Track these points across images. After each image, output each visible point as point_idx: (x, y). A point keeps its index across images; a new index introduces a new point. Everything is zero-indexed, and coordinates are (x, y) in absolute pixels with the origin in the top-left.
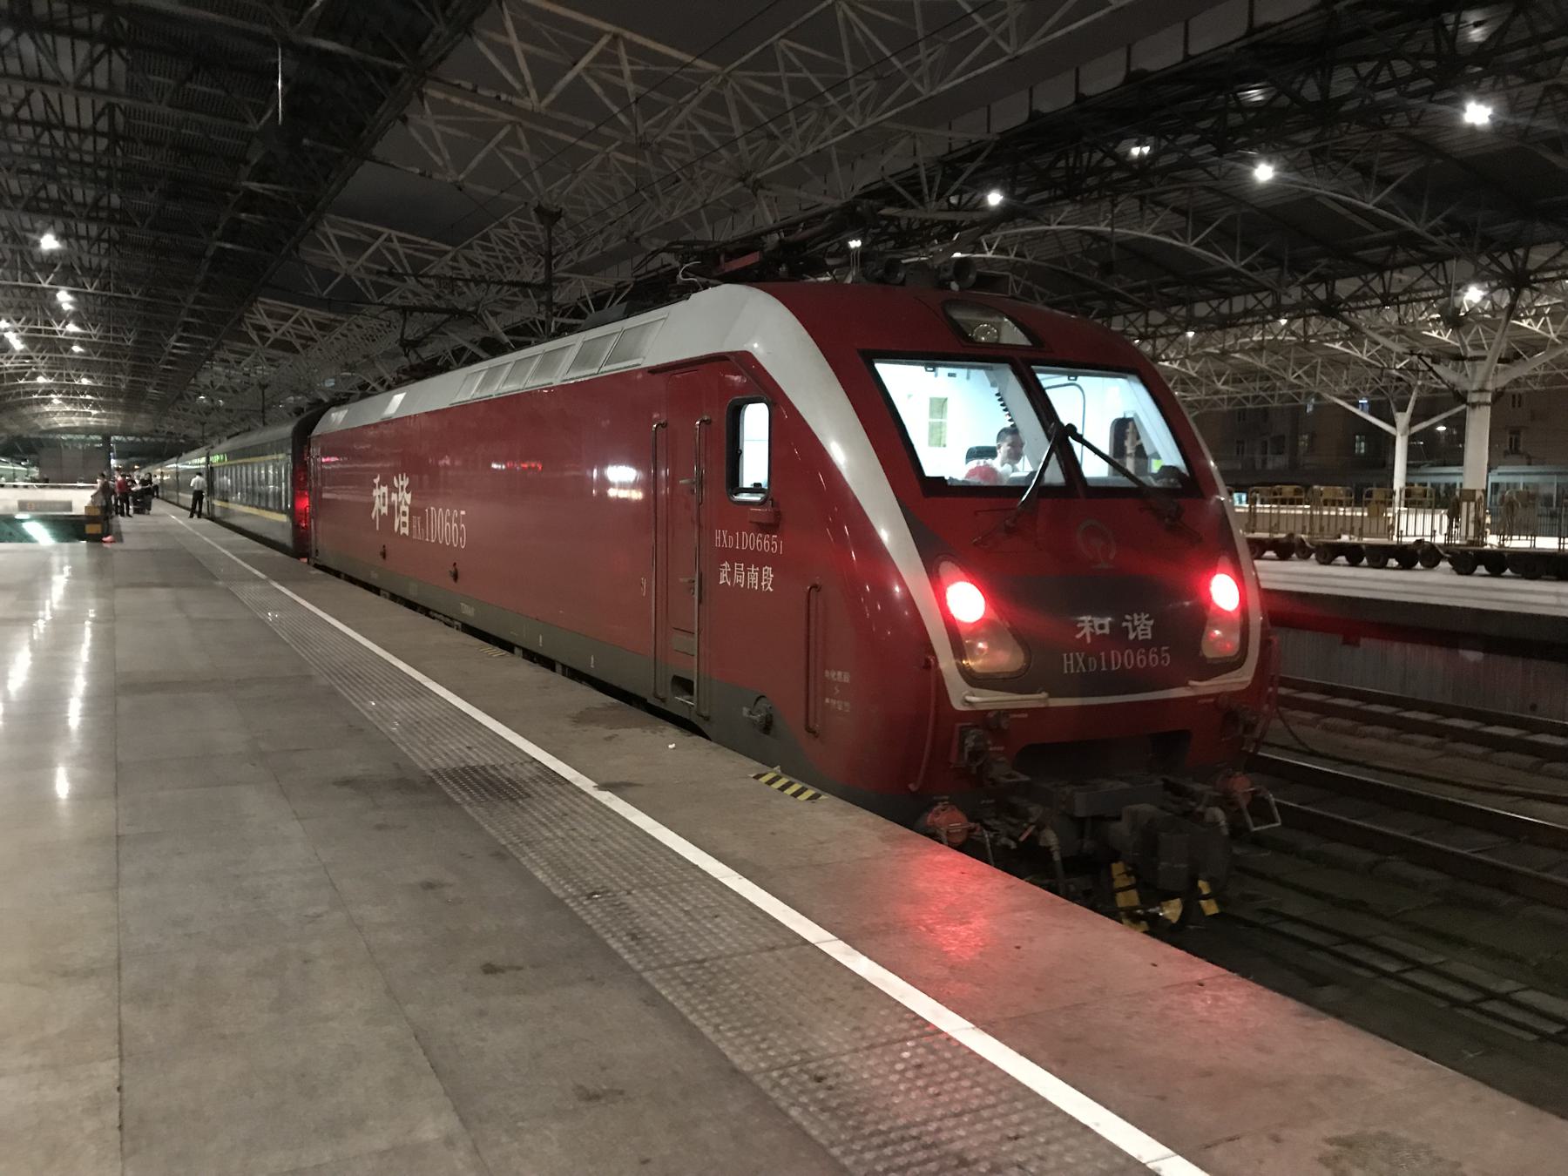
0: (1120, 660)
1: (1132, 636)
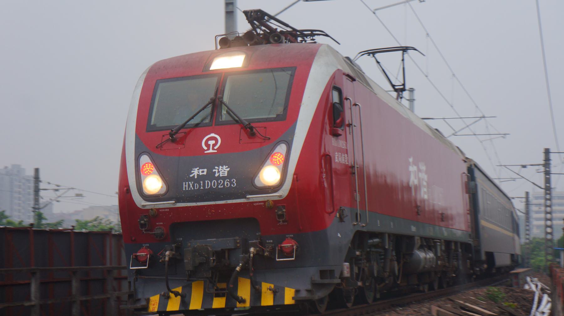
0: (209, 184)
1: (217, 175)
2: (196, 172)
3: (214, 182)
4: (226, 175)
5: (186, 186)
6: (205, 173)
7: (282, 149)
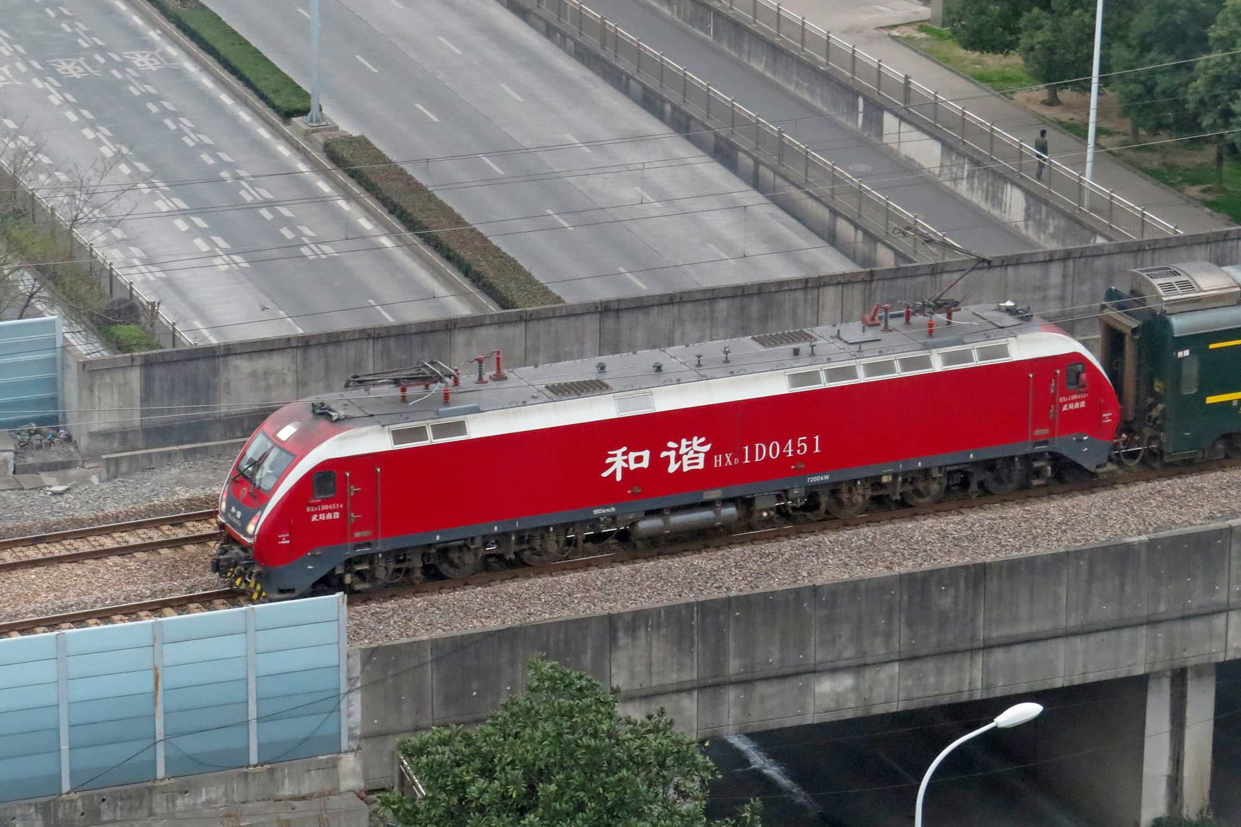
1: (672, 468)
3: (775, 446)
4: (701, 466)
6: (645, 464)
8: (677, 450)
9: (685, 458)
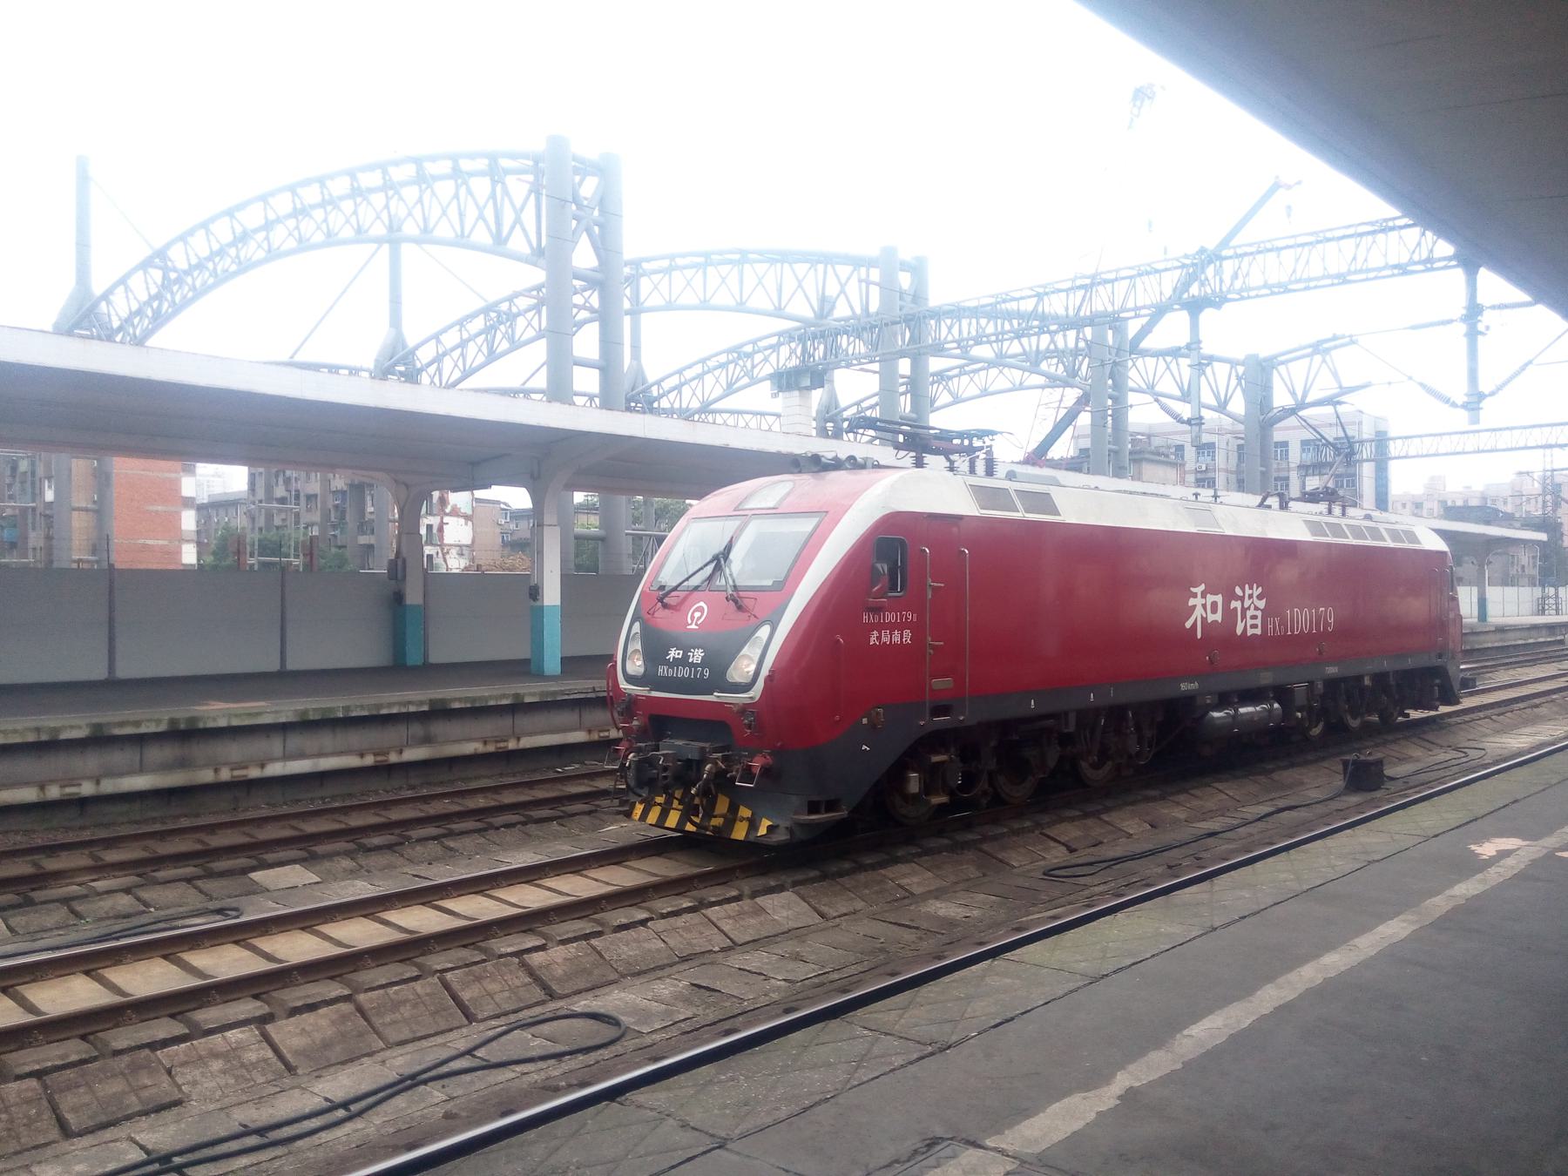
0: (684, 672)
2: (674, 654)
5: (663, 671)
6: (1218, 617)
7: (764, 632)
8: (1242, 599)
9: (1249, 614)
